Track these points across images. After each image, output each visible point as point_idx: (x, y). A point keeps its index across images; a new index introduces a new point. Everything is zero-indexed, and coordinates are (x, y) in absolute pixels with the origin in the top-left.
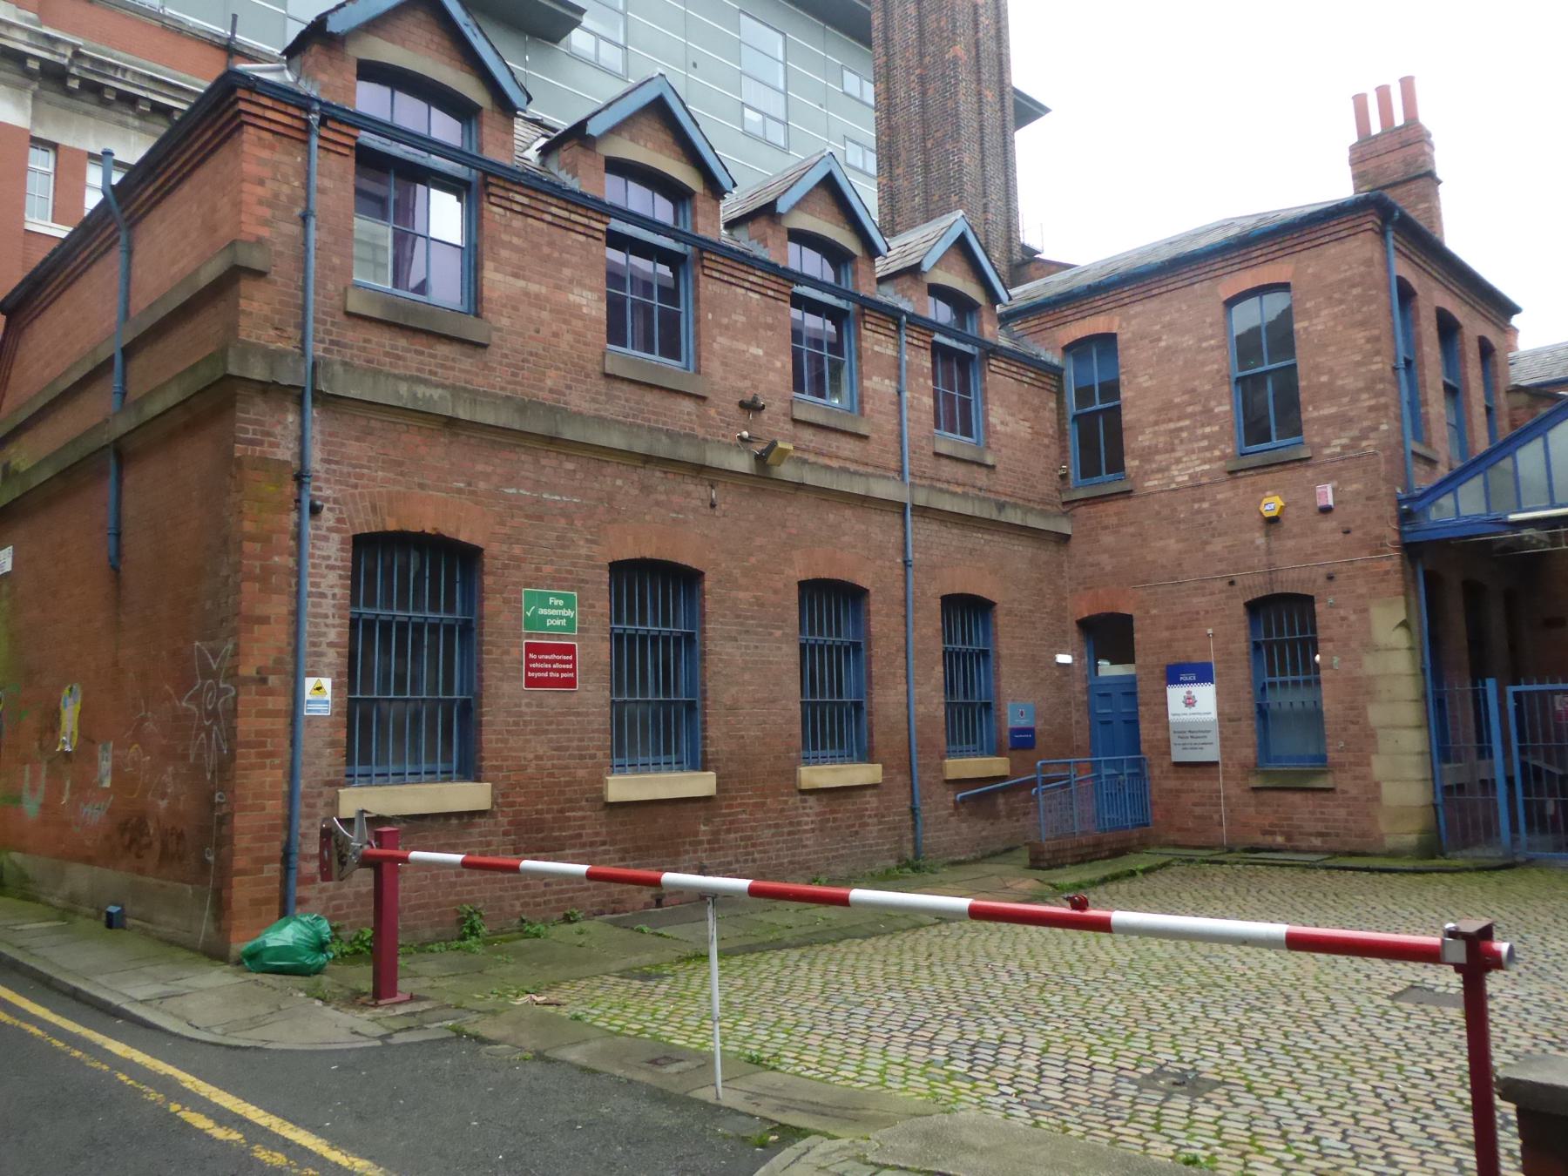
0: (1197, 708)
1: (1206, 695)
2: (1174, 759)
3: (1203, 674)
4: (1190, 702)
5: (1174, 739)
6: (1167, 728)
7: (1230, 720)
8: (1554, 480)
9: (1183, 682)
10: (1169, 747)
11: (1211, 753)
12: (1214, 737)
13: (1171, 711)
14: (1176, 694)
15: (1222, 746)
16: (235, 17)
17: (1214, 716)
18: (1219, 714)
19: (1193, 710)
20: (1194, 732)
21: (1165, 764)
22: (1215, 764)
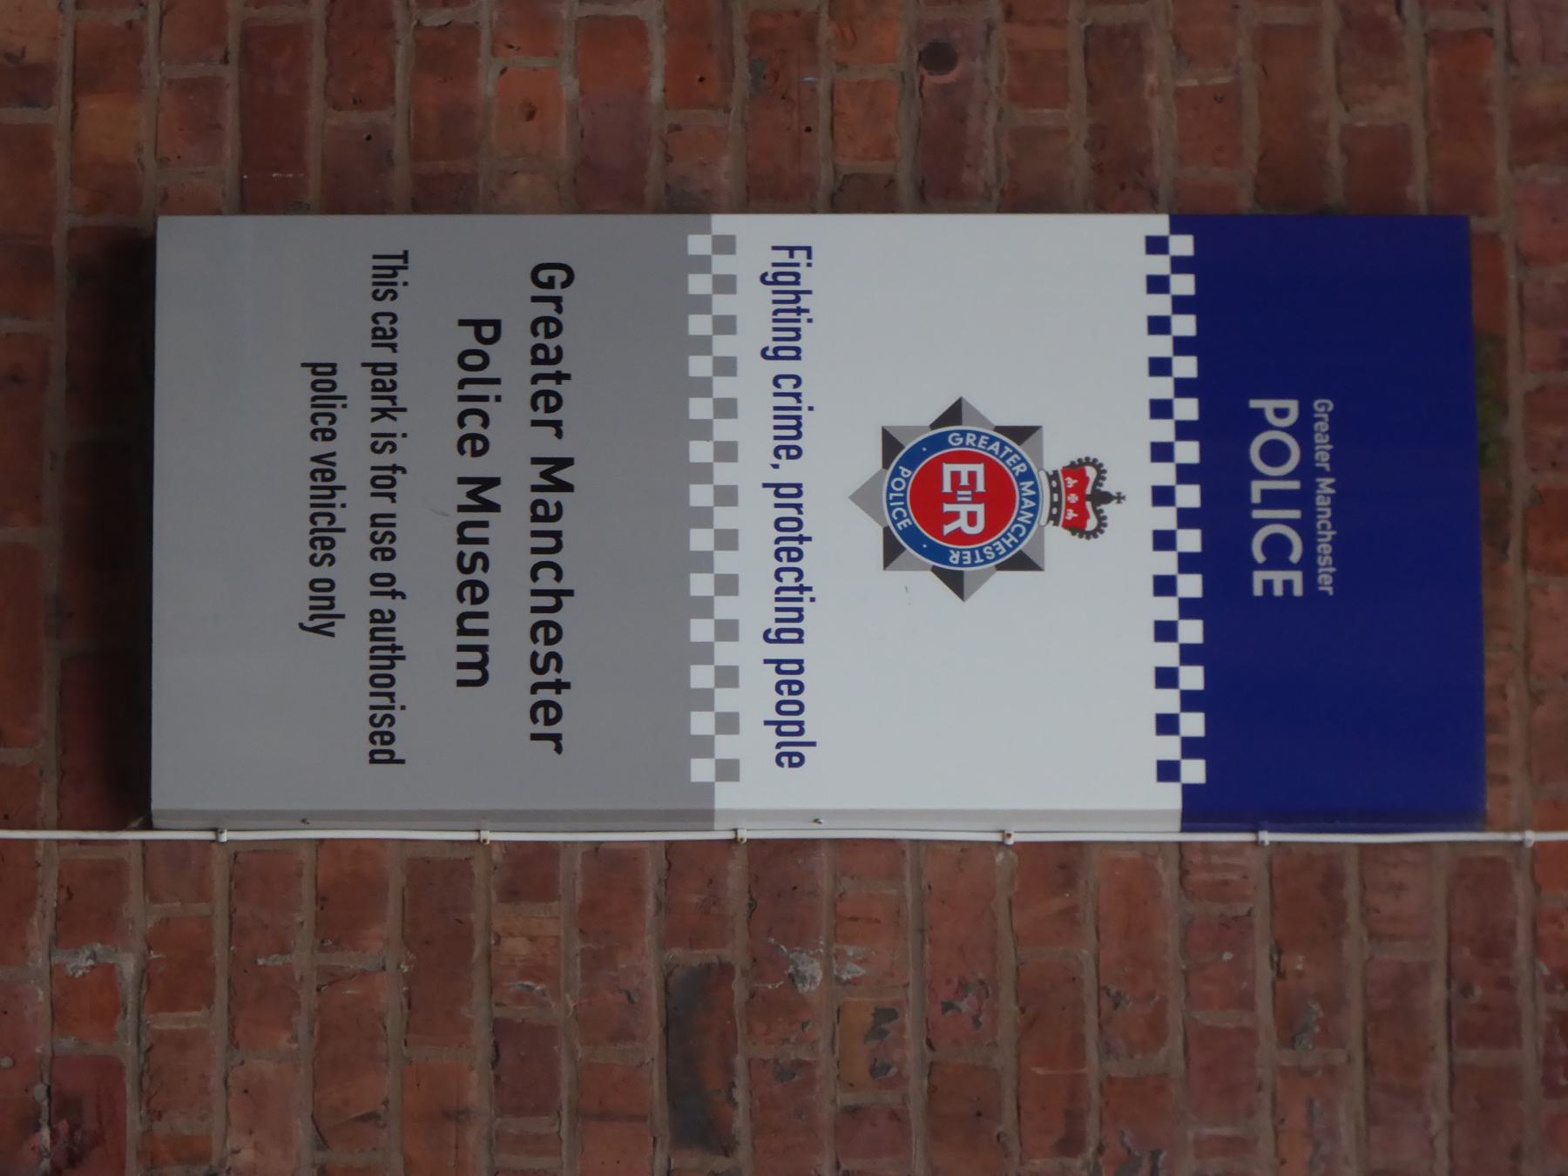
0: (868, 602)
1: (1041, 710)
2: (186, 252)
3: (1308, 697)
4: (959, 499)
5: (470, 261)
6: (616, 179)
7: (693, 1004)
8: (360, 699)
9: (1222, 432)
10: (348, 195)
11: (254, 726)
12: (468, 778)
13: (842, 242)
14: (1061, 322)
15: (347, 884)
16: (774, 248)
17: (756, 797)
18: (779, 864)
19: (846, 537)
20: (535, 536)
21: (128, 127)
22: (114, 763)
